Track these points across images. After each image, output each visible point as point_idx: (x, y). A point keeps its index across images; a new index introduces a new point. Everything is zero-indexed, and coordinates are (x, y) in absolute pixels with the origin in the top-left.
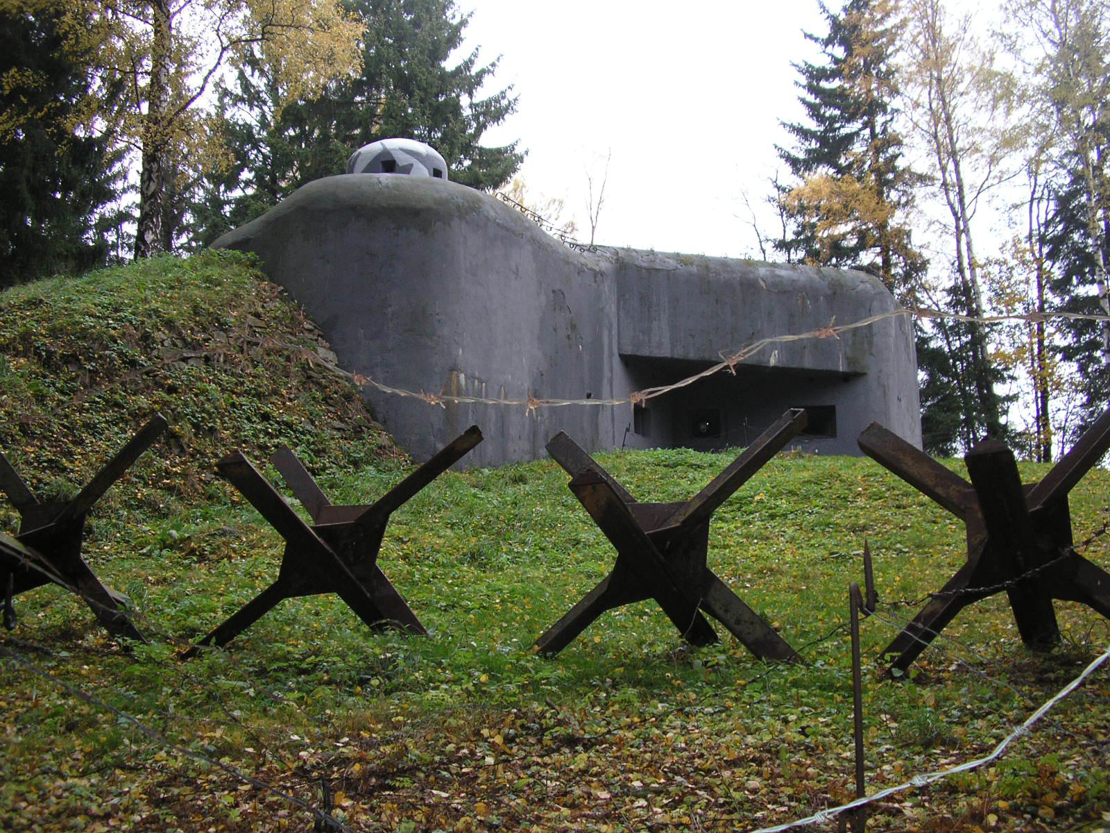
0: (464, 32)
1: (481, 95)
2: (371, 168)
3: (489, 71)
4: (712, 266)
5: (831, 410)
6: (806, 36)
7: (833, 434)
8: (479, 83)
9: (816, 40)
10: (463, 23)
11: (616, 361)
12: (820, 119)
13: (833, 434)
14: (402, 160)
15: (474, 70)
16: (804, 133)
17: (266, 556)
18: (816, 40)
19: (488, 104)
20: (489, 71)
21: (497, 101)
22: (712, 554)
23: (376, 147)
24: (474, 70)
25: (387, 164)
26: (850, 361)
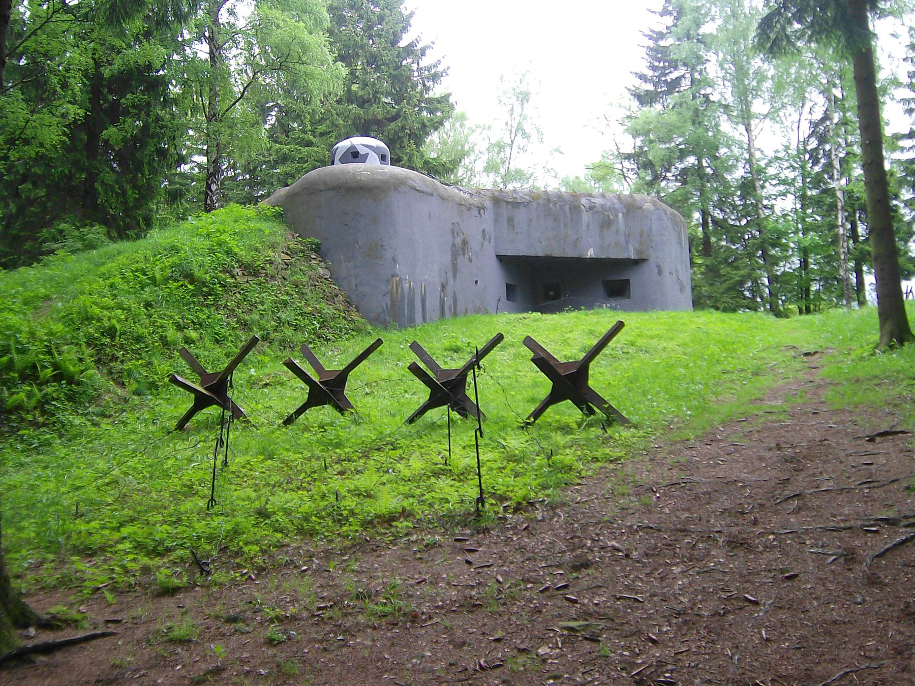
0: (412, 21)
1: (424, 63)
2: (343, 160)
3: (429, 47)
4: (551, 198)
5: (628, 281)
6: (649, 10)
7: (629, 297)
8: (423, 54)
9: (654, 12)
10: (411, 15)
11: (494, 262)
12: (653, 68)
13: (629, 297)
14: (362, 151)
15: (419, 46)
16: (642, 77)
17: (299, 392)
18: (654, 12)
19: (429, 69)
20: (429, 47)
21: (435, 66)
22: (591, 383)
23: (345, 144)
24: (419, 46)
25: (354, 155)
26: (638, 252)
